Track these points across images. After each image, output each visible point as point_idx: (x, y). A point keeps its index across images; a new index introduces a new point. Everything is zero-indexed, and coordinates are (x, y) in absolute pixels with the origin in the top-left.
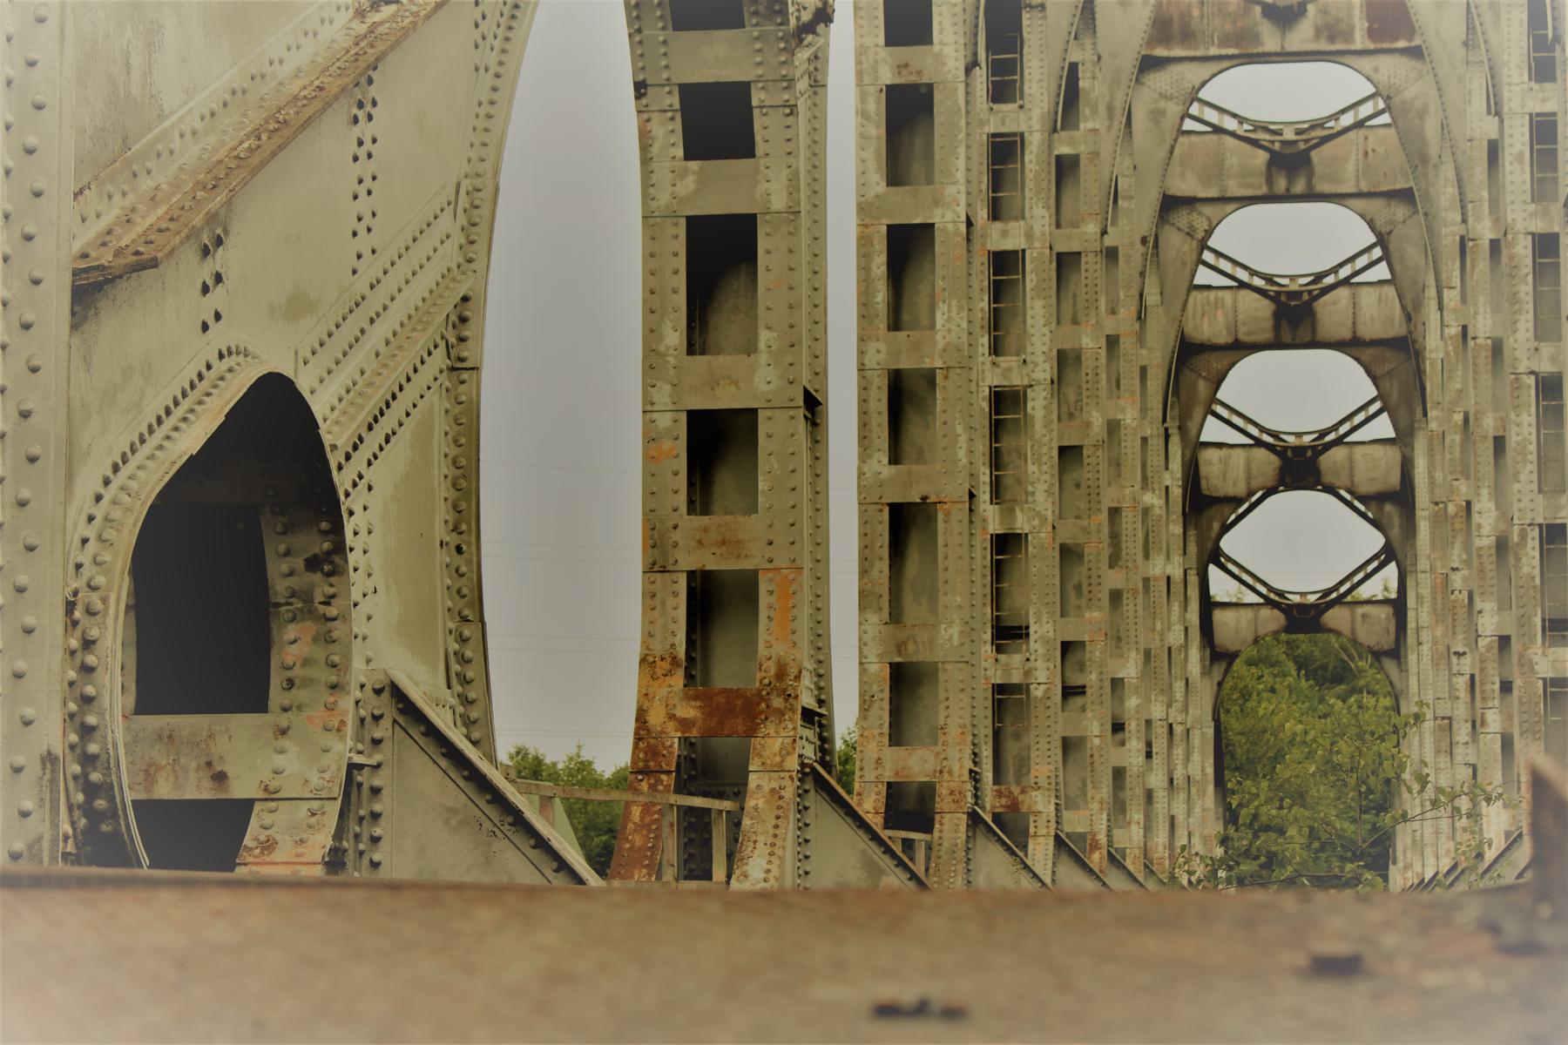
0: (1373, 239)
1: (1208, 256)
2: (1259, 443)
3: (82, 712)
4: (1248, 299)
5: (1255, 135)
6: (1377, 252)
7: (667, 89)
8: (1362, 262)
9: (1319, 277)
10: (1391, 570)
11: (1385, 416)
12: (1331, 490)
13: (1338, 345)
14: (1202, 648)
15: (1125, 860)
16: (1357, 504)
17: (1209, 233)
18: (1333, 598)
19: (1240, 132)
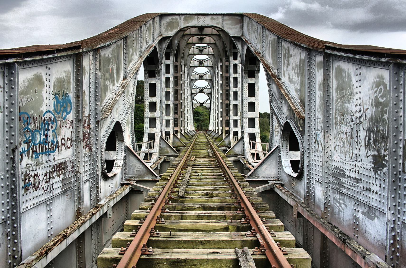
3: (10, 139)
9: (203, 74)
10: (210, 100)
12: (204, 93)
13: (205, 80)
15: (170, 37)
18: (205, 102)
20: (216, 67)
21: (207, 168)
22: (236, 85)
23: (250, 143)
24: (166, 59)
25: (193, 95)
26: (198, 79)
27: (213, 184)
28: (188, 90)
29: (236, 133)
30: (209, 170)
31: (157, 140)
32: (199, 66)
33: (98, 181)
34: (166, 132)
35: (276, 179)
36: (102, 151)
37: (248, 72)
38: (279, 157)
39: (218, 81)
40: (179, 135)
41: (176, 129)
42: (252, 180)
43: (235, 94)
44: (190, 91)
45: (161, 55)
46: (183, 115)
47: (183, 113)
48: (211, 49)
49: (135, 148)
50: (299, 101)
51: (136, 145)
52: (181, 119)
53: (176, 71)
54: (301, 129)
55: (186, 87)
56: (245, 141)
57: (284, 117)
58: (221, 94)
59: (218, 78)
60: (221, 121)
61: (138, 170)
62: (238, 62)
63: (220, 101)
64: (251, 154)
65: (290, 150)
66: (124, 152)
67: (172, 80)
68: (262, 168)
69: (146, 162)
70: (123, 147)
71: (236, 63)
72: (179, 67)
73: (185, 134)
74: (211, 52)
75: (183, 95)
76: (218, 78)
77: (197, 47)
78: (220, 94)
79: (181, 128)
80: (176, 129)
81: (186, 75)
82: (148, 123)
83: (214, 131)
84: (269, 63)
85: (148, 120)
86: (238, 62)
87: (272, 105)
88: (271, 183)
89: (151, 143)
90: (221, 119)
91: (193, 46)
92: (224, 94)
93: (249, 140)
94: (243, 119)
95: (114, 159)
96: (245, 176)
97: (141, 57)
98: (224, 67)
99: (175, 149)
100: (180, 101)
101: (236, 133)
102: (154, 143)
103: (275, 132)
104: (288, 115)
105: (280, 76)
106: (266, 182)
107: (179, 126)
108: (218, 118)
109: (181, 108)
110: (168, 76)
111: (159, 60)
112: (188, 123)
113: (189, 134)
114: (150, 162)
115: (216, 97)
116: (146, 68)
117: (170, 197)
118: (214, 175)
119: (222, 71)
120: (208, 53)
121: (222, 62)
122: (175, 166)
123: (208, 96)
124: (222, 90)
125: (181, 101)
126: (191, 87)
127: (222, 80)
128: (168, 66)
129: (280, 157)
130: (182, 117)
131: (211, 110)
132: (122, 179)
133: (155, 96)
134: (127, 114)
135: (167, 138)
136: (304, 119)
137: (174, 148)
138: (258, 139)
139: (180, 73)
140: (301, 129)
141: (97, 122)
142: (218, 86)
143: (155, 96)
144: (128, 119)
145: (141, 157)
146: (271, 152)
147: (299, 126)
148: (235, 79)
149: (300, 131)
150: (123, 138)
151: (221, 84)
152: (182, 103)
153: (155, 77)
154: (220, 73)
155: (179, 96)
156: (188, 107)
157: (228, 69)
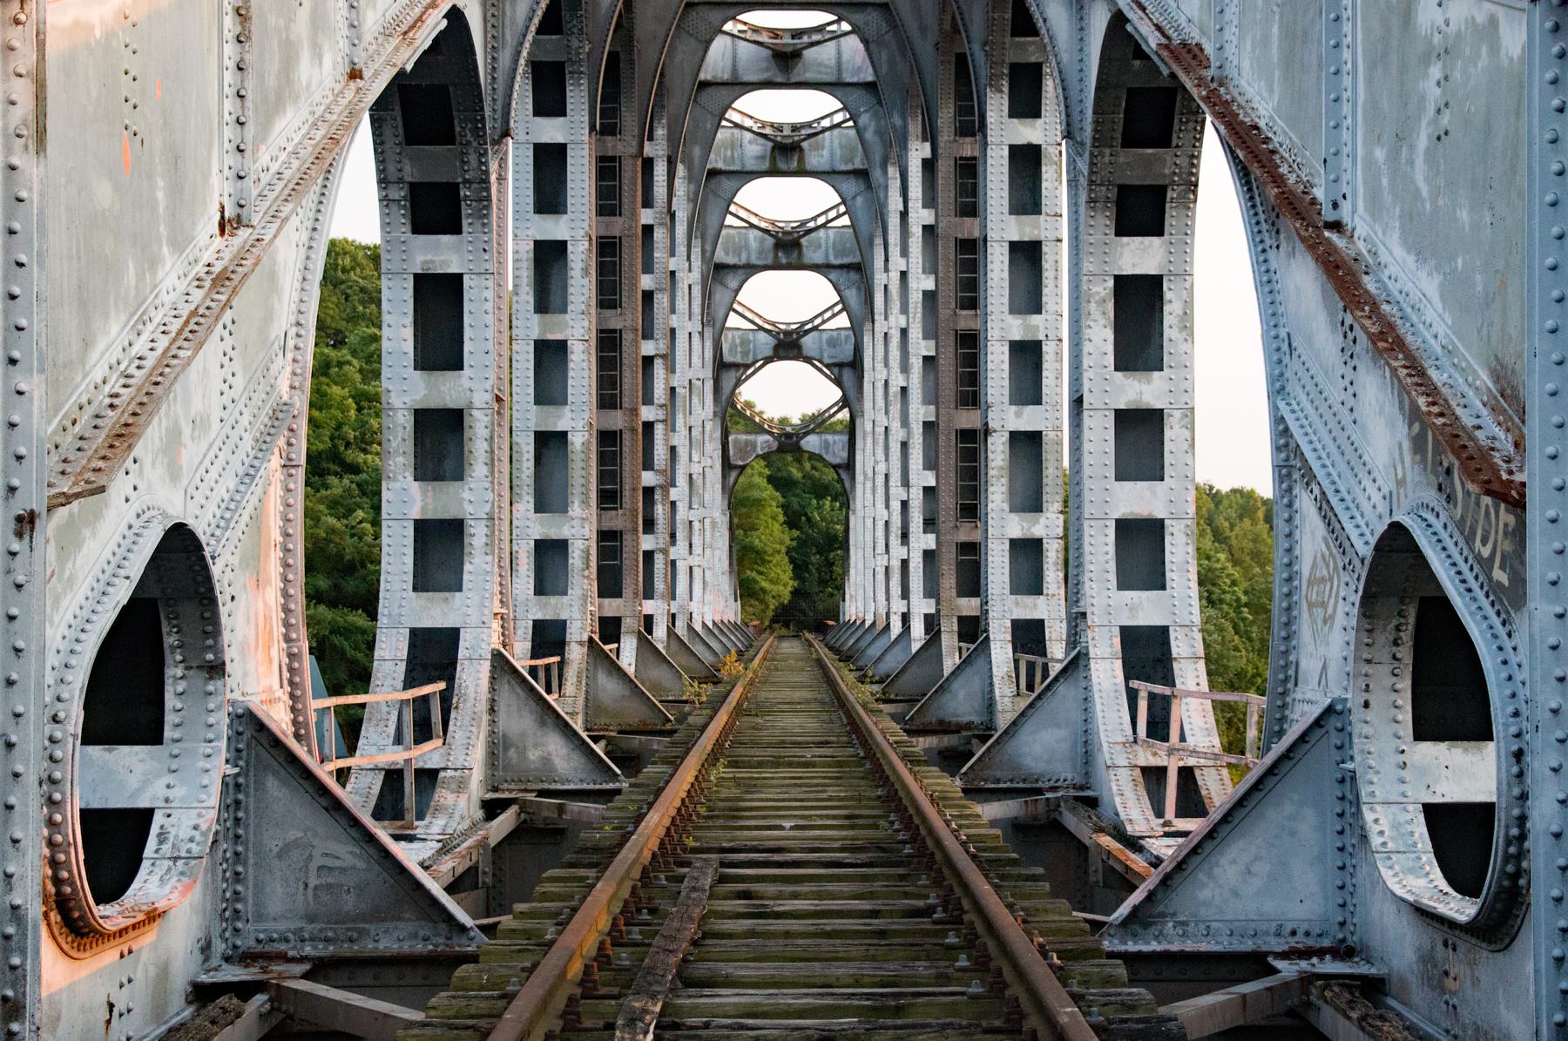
1: (736, 306)
2: (761, 328)
4: (762, 336)
6: (842, 209)
8: (832, 214)
11: (844, 313)
12: (808, 360)
19: (755, 129)
20: (893, 172)
21: (824, 778)
22: (1029, 299)
23: (1132, 696)
24: (539, 111)
25: (729, 378)
26: (769, 261)
27: (868, 969)
28: (696, 339)
29: (1029, 635)
30: (838, 878)
31: (473, 677)
32: (774, 172)
33: (16, 961)
34: (538, 625)
35: (1326, 943)
36: (52, 740)
37: (1113, 194)
38: (1342, 781)
39: (904, 274)
40: (628, 653)
41: (612, 607)
42: (1145, 948)
43: (1027, 355)
44: (709, 344)
45: (499, 75)
46: (660, 511)
47: (658, 496)
49: (306, 725)
50: (1485, 378)
51: (322, 712)
52: (647, 543)
53: (608, 203)
54: (1500, 576)
55: (683, 317)
56: (1095, 680)
57: (1376, 498)
59: (905, 253)
60: (928, 555)
61: (329, 886)
62: (1043, 131)
63: (920, 412)
64: (1138, 771)
65: (1419, 736)
66: (224, 755)
67: (581, 258)
68: (1223, 861)
69: (397, 838)
70: (222, 720)
71: (1035, 141)
72: (631, 173)
73: (674, 645)
74: (860, 70)
75: (659, 368)
76: (905, 253)
77: (756, 30)
78: (916, 364)
79: (649, 607)
80: (612, 607)
81: (681, 229)
82: (409, 559)
83: (880, 625)
84: (1262, 124)
85: (410, 541)
86: (1043, 131)
87: (1289, 419)
88: (1288, 969)
89: (425, 699)
90: (930, 541)
91: (728, 27)
92: (947, 363)
93: (1127, 679)
94: (1079, 530)
95: (143, 803)
96: (1097, 926)
97: (355, 74)
98: (945, 168)
99: (598, 749)
100: (634, 412)
101: (1029, 635)
102: (446, 698)
103: (1311, 605)
104: (1401, 483)
105: (1346, 207)
106: (1256, 964)
107: (628, 591)
108: (905, 537)
109: (648, 465)
110: (553, 228)
111: (488, 112)
112: (697, 573)
113: (698, 649)
114: (419, 832)
115: (894, 389)
116: (391, 168)
118: (874, 914)
119: (930, 201)
120: (831, 78)
121: (930, 134)
123: (838, 382)
124: (930, 333)
125: (647, 413)
126: (712, 321)
127: (931, 267)
128: (550, 160)
129: (1349, 780)
130: (649, 526)
131: (859, 478)
132: (206, 949)
133: (458, 365)
134: (249, 476)
135: (548, 668)
136: (1523, 496)
137: (596, 739)
138: (1190, 674)
139: (634, 216)
140: (1500, 576)
141: (19, 519)
142: (904, 310)
143: (458, 365)
144: (257, 519)
145: (359, 796)
146: (1278, 749)
147: (1486, 552)
148: (1027, 255)
149: (1493, 589)
150: (217, 649)
151: (925, 293)
152: (649, 427)
153: (457, 230)
154: (921, 216)
155: (630, 378)
156: (696, 457)
157: (975, 186)
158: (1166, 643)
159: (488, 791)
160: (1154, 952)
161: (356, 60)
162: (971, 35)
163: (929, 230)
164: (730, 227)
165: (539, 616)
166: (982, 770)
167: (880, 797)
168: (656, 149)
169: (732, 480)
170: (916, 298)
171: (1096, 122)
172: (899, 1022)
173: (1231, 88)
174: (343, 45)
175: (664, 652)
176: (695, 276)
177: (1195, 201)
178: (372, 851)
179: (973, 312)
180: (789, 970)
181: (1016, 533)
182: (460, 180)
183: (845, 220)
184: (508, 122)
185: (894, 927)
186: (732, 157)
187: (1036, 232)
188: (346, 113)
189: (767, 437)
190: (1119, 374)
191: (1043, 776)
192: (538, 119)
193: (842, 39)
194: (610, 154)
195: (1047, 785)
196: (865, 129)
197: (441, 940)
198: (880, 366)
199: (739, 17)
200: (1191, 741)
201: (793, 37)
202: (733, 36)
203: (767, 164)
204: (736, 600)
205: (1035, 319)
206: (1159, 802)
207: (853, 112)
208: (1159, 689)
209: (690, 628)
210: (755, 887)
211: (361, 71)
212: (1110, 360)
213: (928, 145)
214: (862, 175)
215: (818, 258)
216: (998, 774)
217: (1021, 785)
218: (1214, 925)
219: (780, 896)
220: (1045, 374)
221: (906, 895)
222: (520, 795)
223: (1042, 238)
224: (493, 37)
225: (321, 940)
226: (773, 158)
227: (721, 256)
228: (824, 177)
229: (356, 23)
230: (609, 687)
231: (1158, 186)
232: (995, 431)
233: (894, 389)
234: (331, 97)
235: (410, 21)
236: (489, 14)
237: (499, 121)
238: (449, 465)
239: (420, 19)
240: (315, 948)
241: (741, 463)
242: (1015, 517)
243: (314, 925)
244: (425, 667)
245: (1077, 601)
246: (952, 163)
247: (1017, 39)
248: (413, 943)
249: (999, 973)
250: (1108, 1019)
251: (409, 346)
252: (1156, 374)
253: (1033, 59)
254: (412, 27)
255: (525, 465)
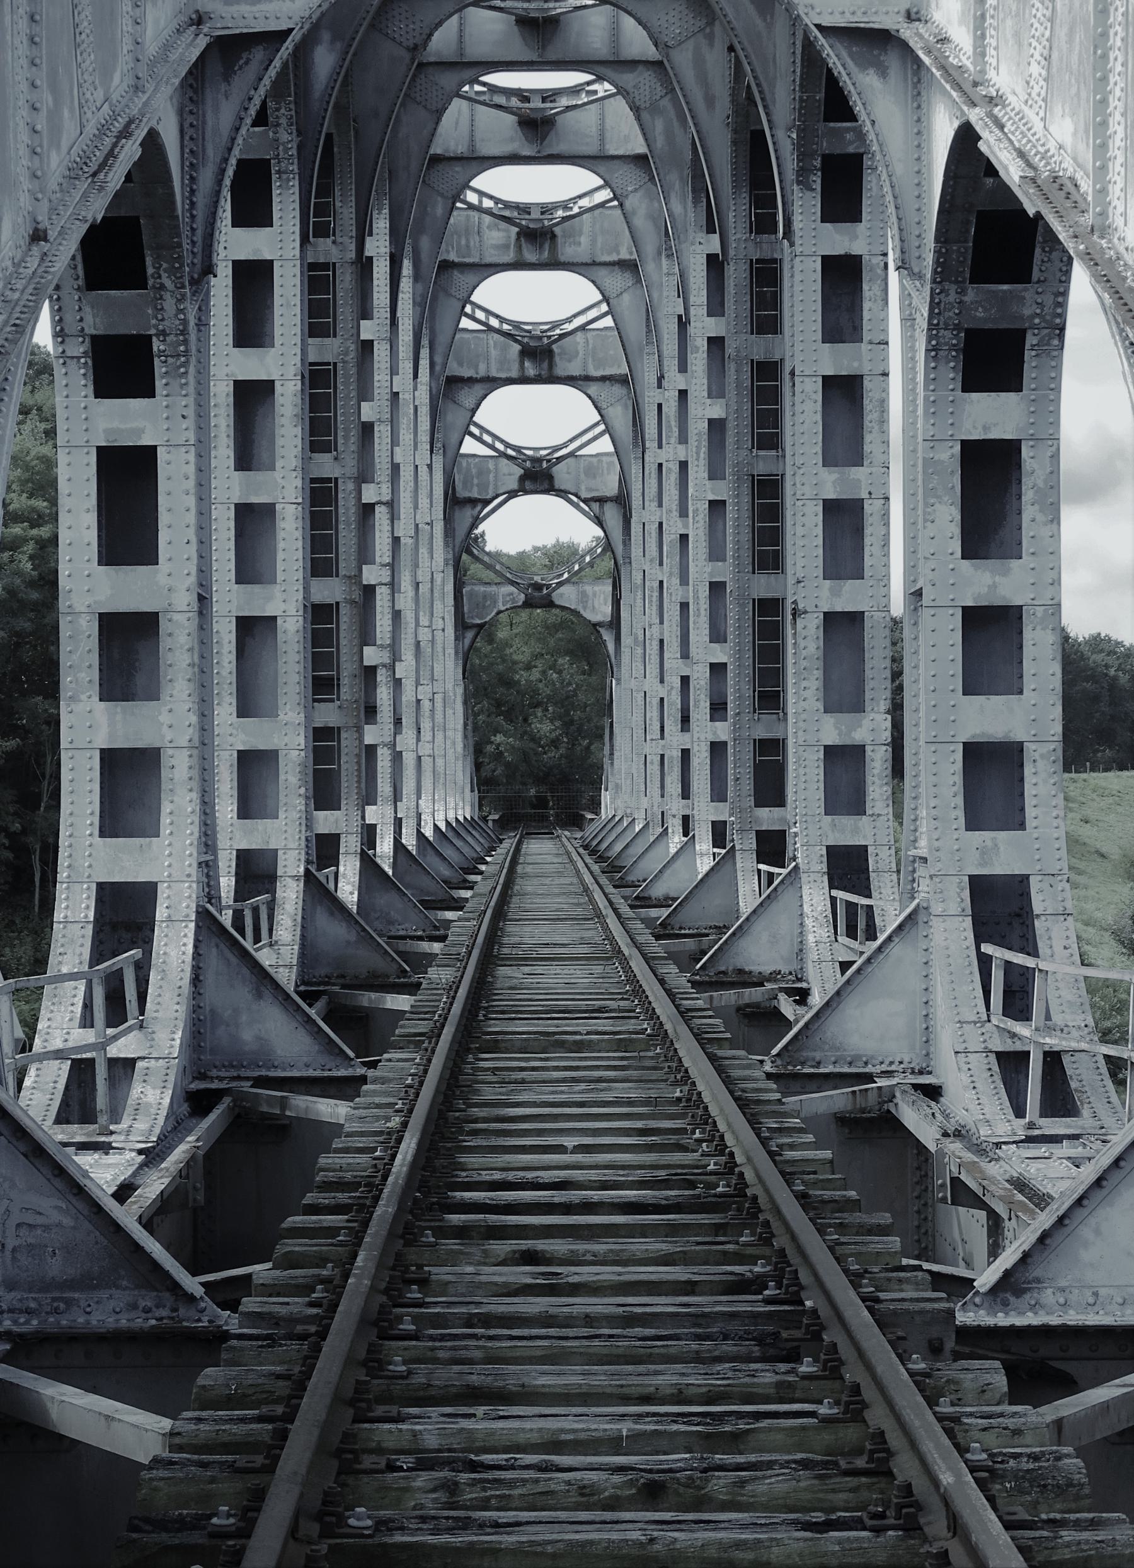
0: (600, 297)
1: (473, 429)
5: (514, 333)
7: (86, 450)
12: (562, 493)
14: (446, 544)
16: (582, 504)
17: (474, 411)
23: (985, 962)
25: (464, 516)
26: (514, 374)
27: (695, 1379)
28: (423, 471)
30: (643, 1231)
32: (519, 265)
39: (683, 394)
41: (326, 821)
42: (1019, 1321)
46: (383, 695)
48: (620, 112)
58: (716, 507)
59: (683, 368)
60: (717, 749)
61: (30, 1247)
63: (701, 570)
64: (993, 1057)
71: (856, 250)
76: (683, 368)
77: (493, 89)
80: (326, 821)
93: (979, 939)
97: (38, 236)
98: (736, 275)
102: (142, 969)
108: (685, 720)
112: (427, 762)
115: (671, 536)
116: (70, 318)
117: (342, 1521)
118: (690, 1288)
120: (592, 149)
122: (342, 1197)
123: (599, 522)
127: (716, 391)
130: (371, 712)
142: (683, 439)
158: (1025, 895)
159: (194, 1078)
160: (1029, 1326)
161: (40, 218)
162: (775, 118)
163: (716, 343)
164: (465, 330)
165: (244, 845)
166: (798, 1050)
167: (679, 1099)
168: (378, 246)
169: (467, 642)
170: (698, 427)
171: (937, 252)
172: (741, 1459)
173: (1116, 240)
174: (25, 200)
175: (390, 873)
176: (423, 396)
177: (1062, 348)
178: (80, 1205)
179: (773, 453)
180: (601, 1378)
181: (832, 738)
182: (153, 331)
183: (608, 322)
184: (210, 257)
185: (718, 1309)
186: (468, 246)
187: (856, 364)
188: (30, 290)
189: (512, 589)
190: (966, 562)
191: (872, 1057)
192: (238, 231)
193: (606, 101)
194: (322, 260)
195: (878, 1069)
196: (634, 213)
197: (164, 1313)
198: (652, 506)
199: (481, 79)
200: (1058, 1019)
201: (544, 100)
202: (469, 99)
203: (512, 254)
204: (472, 791)
205: (856, 473)
206: (1018, 1093)
207: (618, 192)
208: (1019, 959)
209: (420, 835)
210: (541, 1245)
211: (45, 231)
212: (956, 546)
213: (716, 238)
214: (630, 267)
215: (574, 369)
216: (818, 1055)
217: (846, 1069)
218: (1103, 1292)
219: (573, 1260)
220: (867, 541)
221: (727, 1258)
222: (233, 1084)
223: (865, 371)
224: (192, 151)
225: (21, 1311)
226: (519, 248)
227: (455, 369)
228: (582, 269)
229: (39, 173)
230: (334, 931)
231: (1018, 330)
232: (805, 612)
233: (671, 536)
234: (11, 269)
235: (100, 155)
236: (186, 125)
237: (199, 256)
238: (140, 680)
239: (111, 154)
240: (15, 1322)
241: (479, 622)
242: (829, 720)
243: (13, 1294)
244: (114, 927)
245: (915, 841)
246: (747, 266)
247: (832, 124)
248: (133, 1315)
249: (856, 1389)
250: (992, 1456)
251: (92, 536)
252: (1014, 563)
253: (851, 149)
254: (103, 165)
255: (225, 651)
